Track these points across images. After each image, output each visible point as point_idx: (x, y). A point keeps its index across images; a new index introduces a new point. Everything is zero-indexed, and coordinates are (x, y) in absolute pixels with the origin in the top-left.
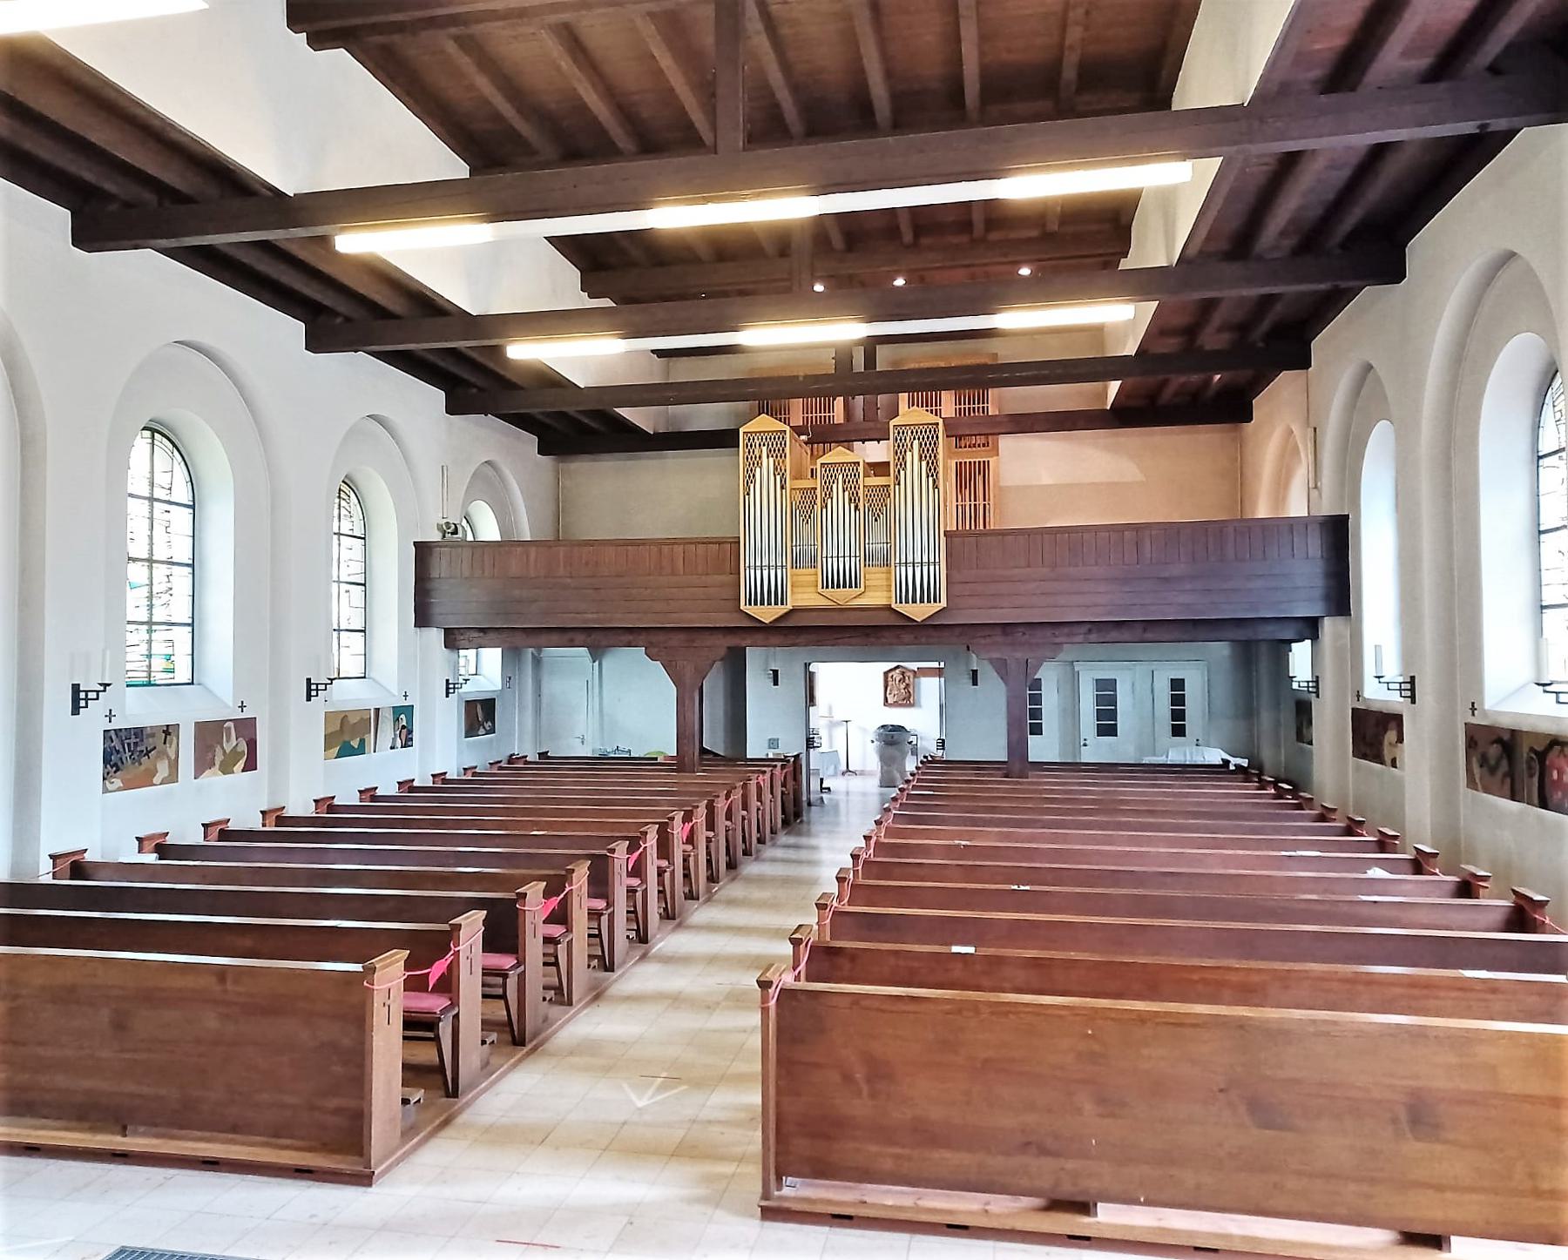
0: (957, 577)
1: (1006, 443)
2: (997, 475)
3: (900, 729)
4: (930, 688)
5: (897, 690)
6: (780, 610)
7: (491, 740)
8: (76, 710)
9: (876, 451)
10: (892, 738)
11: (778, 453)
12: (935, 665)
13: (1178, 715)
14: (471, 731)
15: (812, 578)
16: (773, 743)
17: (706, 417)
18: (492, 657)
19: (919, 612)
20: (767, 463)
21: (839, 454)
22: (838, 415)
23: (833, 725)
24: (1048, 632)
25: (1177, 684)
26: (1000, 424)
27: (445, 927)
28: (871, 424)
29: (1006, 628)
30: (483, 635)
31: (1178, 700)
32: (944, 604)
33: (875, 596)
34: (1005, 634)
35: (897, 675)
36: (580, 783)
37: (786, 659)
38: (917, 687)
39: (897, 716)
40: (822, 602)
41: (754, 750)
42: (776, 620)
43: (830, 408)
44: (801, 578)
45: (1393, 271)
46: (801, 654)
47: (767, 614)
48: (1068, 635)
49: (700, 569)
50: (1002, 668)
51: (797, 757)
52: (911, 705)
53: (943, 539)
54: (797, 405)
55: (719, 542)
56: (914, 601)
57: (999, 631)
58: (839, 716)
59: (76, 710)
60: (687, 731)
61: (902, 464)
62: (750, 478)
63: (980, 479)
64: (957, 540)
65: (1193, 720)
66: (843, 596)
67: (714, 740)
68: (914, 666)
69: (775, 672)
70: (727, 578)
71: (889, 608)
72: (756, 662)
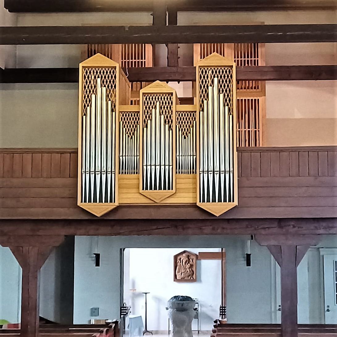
0: (246, 183)
1: (271, 87)
2: (264, 109)
3: (187, 299)
4: (210, 268)
5: (184, 268)
6: (110, 206)
9: (179, 89)
10: (183, 307)
11: (110, 85)
12: (218, 250)
15: (135, 182)
16: (95, 312)
17: (48, 56)
19: (217, 209)
20: (101, 91)
21: (157, 86)
22: (149, 62)
23: (136, 296)
24: (312, 226)
26: (265, 73)
28: (174, 69)
29: (281, 222)
32: (236, 203)
33: (183, 195)
34: (281, 227)
35: (184, 258)
37: (102, 244)
38: (199, 267)
39: (185, 289)
40: (143, 201)
41: (80, 316)
42: (102, 216)
43: (142, 55)
44: (126, 182)
46: (117, 241)
47: (99, 209)
48: (325, 228)
49: (45, 175)
50: (277, 252)
51: (116, 323)
52: (194, 281)
53: (236, 153)
54: (118, 48)
55: (62, 152)
56: (214, 201)
57: (276, 224)
58: (140, 289)
60: (28, 306)
61: (205, 96)
62: (88, 102)
63: (252, 112)
64: (245, 155)
66: (159, 196)
67: (47, 309)
68: (196, 251)
69: (98, 256)
70: (69, 181)
71: (194, 206)
72: (82, 246)
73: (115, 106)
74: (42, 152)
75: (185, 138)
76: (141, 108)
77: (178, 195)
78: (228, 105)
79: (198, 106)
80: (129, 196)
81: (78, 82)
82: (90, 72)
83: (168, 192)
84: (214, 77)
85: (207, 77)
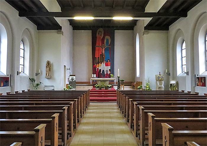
16: (64, 89)
45: (186, 16)
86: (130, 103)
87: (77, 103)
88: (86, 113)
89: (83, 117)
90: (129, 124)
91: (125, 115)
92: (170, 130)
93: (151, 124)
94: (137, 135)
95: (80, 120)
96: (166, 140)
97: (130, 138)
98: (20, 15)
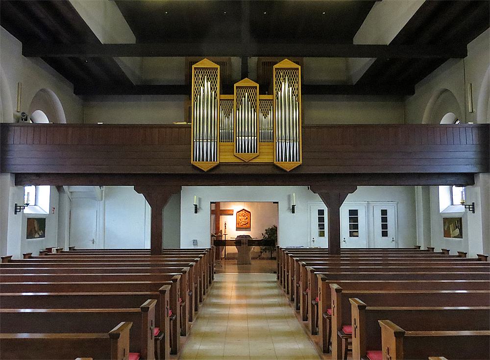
7: (42, 241)
8: (196, 212)
13: (384, 227)
14: (30, 235)
15: (232, 147)
16: (195, 242)
18: (45, 191)
19: (288, 166)
25: (384, 212)
27: (105, 336)
30: (37, 179)
31: (384, 220)
36: (398, 254)
47: (205, 166)
59: (196, 212)
65: (391, 229)
66: (247, 157)
73: (216, 95)
74: (166, 128)
75: (265, 118)
76: (235, 97)
77: (260, 157)
78: (295, 95)
79: (275, 96)
80: (227, 157)
81: (233, 94)
82: (199, 72)
83: (253, 155)
84: (205, 75)
85: (283, 76)
86: (301, 271)
87: (178, 287)
88: (197, 318)
89: (190, 334)
90: (320, 337)
91: (315, 325)
92: (337, 290)
93: (336, 302)
94: (305, 319)
95: (182, 346)
96: (389, 357)
97: (305, 346)
98: (26, 53)
